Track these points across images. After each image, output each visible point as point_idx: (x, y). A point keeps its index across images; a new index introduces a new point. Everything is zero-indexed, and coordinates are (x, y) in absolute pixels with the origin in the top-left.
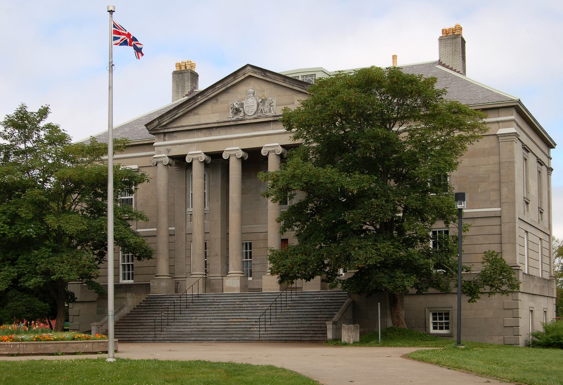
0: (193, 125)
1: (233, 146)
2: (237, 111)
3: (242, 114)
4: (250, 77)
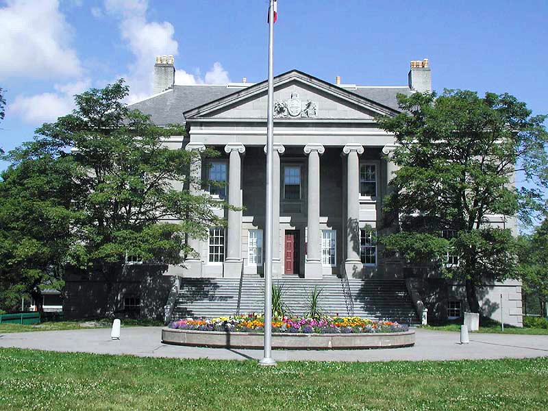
0: (321, 119)
1: (314, 143)
2: (282, 110)
3: (286, 113)
4: (295, 82)
